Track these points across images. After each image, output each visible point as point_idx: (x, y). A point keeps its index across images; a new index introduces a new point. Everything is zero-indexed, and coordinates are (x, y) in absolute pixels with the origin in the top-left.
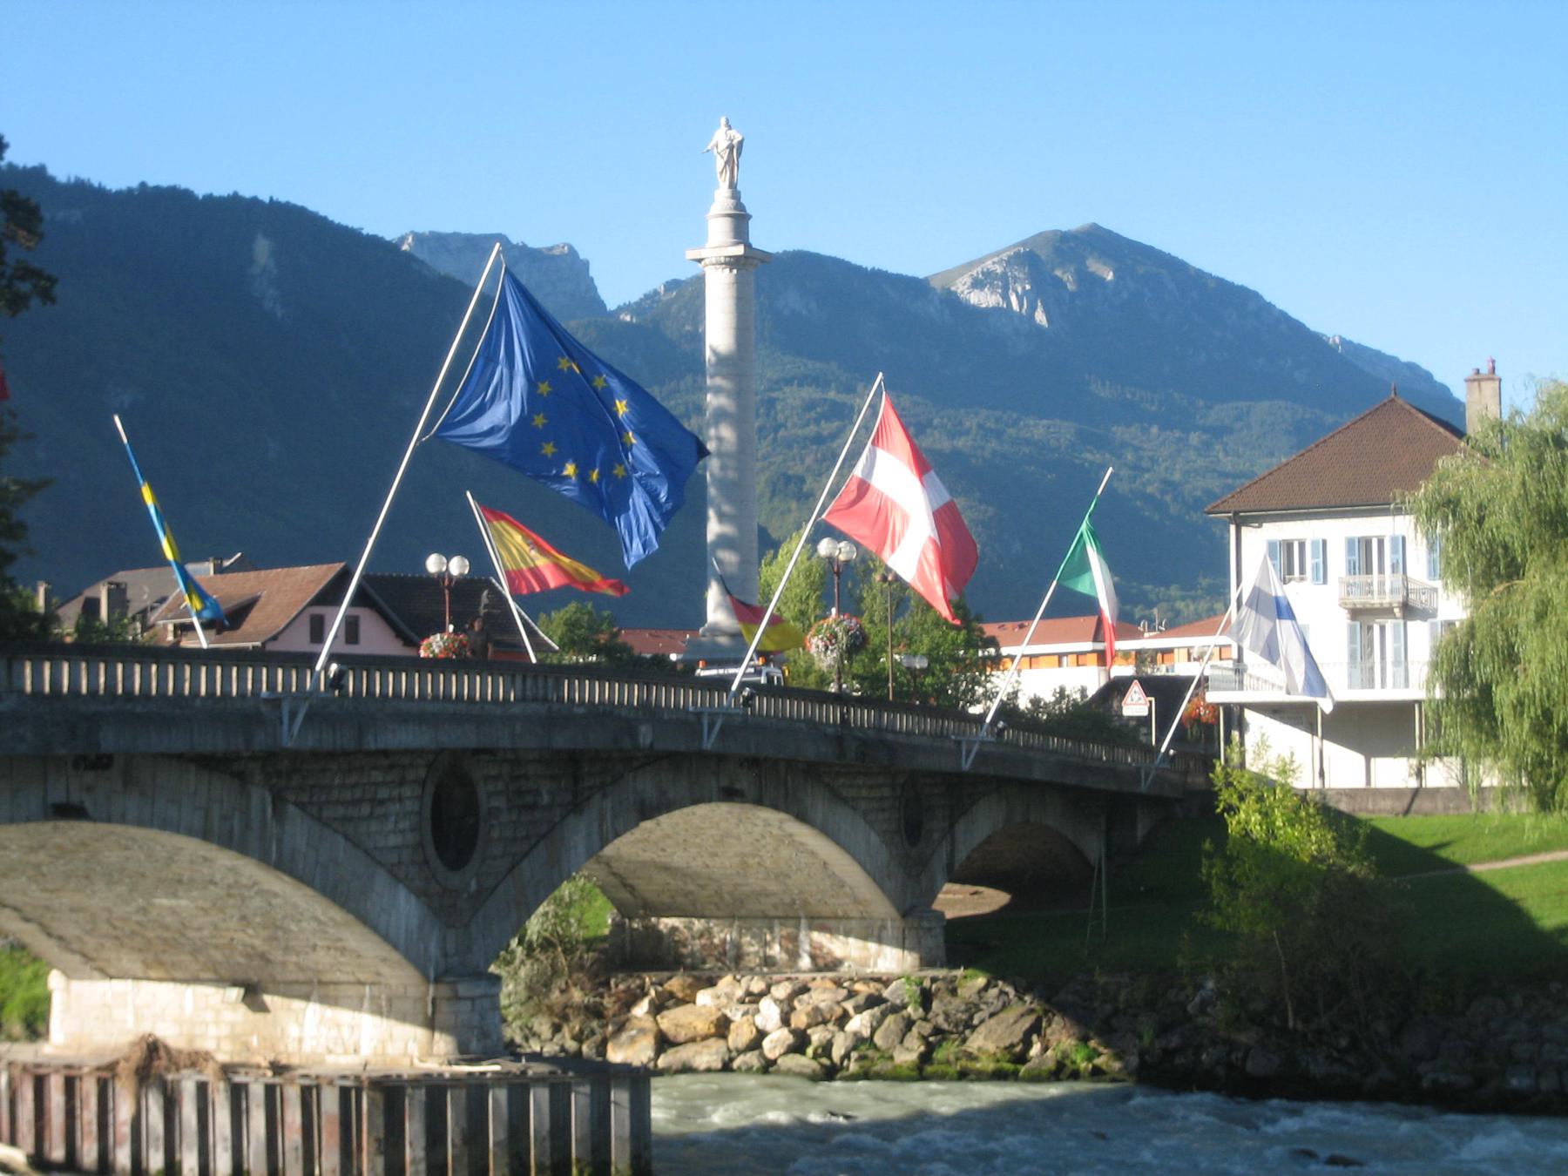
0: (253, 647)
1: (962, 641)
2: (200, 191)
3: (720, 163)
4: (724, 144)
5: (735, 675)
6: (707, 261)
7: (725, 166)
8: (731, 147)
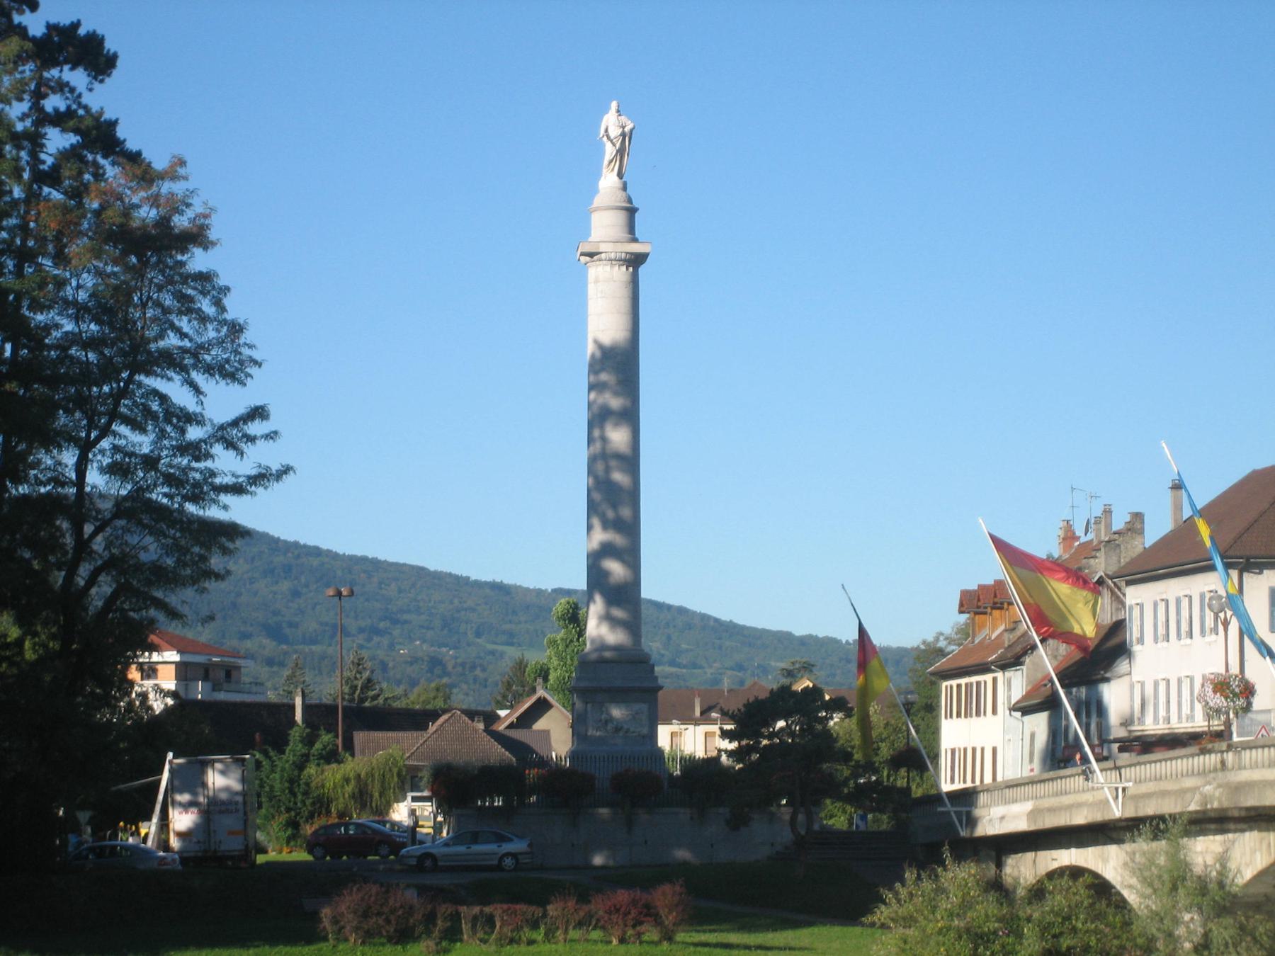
0: (517, 718)
1: (59, 270)
2: (820, 635)
3: (610, 151)
4: (615, 132)
5: (946, 806)
6: (603, 256)
7: (616, 154)
8: (623, 135)
